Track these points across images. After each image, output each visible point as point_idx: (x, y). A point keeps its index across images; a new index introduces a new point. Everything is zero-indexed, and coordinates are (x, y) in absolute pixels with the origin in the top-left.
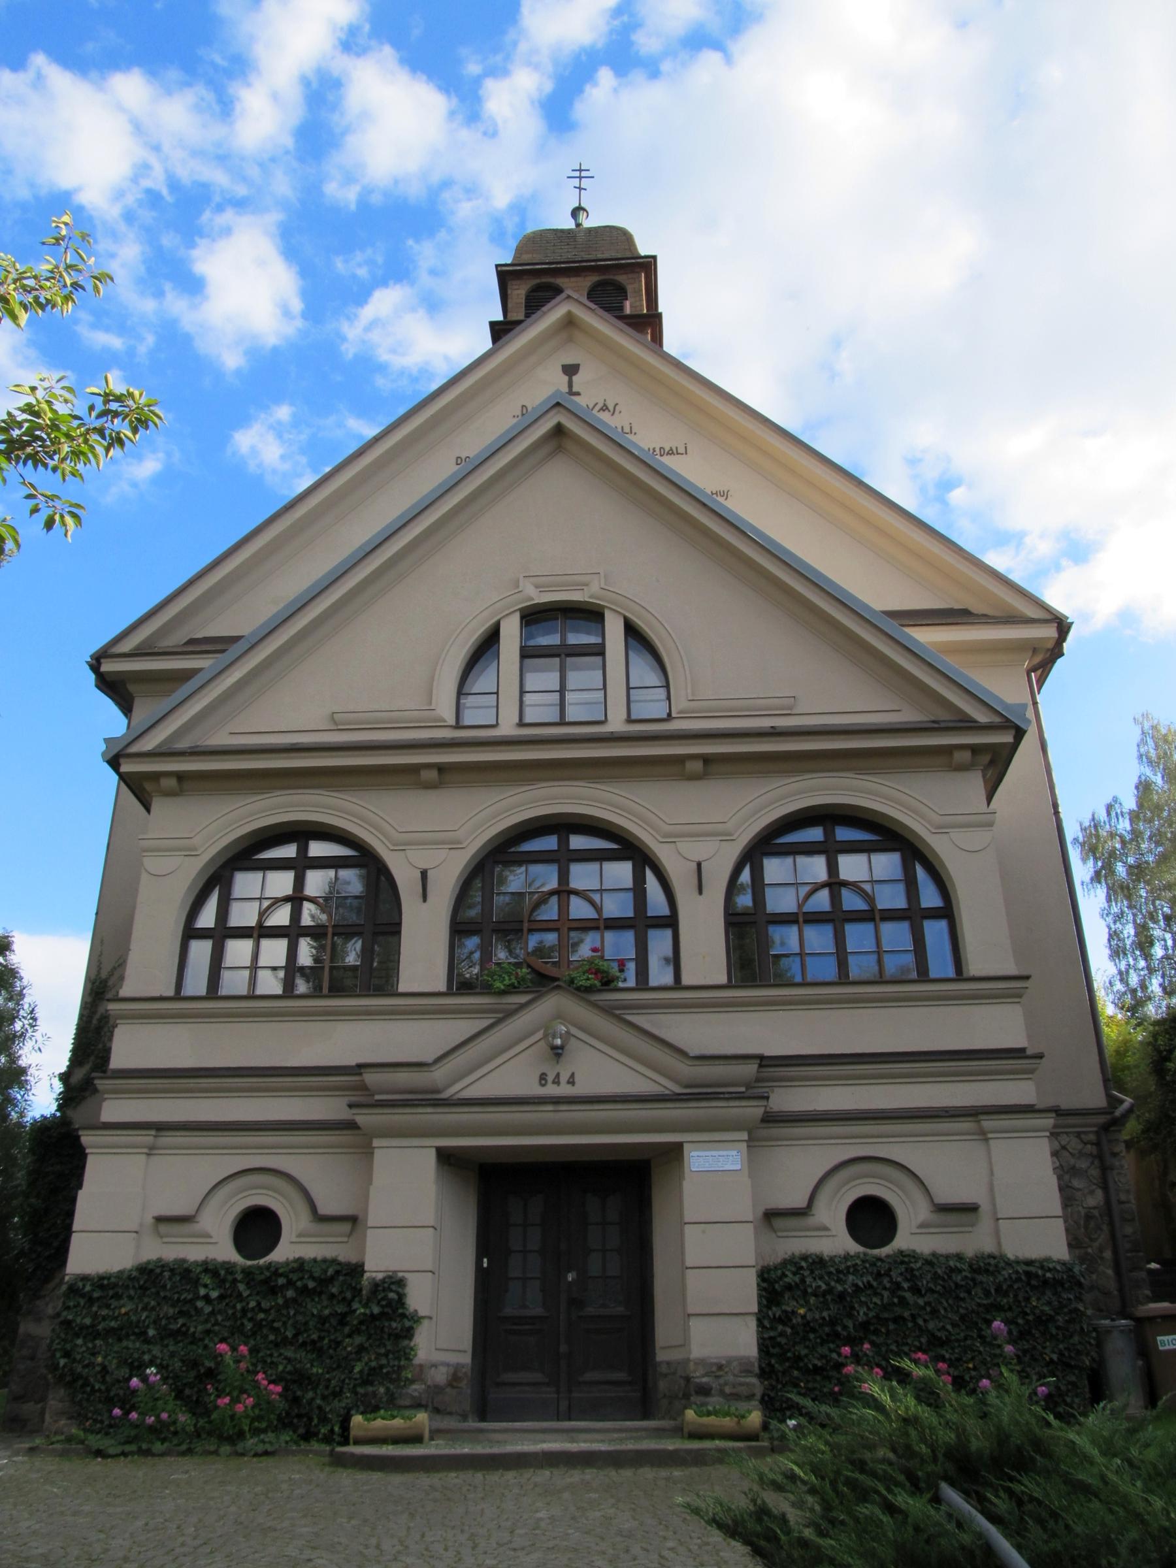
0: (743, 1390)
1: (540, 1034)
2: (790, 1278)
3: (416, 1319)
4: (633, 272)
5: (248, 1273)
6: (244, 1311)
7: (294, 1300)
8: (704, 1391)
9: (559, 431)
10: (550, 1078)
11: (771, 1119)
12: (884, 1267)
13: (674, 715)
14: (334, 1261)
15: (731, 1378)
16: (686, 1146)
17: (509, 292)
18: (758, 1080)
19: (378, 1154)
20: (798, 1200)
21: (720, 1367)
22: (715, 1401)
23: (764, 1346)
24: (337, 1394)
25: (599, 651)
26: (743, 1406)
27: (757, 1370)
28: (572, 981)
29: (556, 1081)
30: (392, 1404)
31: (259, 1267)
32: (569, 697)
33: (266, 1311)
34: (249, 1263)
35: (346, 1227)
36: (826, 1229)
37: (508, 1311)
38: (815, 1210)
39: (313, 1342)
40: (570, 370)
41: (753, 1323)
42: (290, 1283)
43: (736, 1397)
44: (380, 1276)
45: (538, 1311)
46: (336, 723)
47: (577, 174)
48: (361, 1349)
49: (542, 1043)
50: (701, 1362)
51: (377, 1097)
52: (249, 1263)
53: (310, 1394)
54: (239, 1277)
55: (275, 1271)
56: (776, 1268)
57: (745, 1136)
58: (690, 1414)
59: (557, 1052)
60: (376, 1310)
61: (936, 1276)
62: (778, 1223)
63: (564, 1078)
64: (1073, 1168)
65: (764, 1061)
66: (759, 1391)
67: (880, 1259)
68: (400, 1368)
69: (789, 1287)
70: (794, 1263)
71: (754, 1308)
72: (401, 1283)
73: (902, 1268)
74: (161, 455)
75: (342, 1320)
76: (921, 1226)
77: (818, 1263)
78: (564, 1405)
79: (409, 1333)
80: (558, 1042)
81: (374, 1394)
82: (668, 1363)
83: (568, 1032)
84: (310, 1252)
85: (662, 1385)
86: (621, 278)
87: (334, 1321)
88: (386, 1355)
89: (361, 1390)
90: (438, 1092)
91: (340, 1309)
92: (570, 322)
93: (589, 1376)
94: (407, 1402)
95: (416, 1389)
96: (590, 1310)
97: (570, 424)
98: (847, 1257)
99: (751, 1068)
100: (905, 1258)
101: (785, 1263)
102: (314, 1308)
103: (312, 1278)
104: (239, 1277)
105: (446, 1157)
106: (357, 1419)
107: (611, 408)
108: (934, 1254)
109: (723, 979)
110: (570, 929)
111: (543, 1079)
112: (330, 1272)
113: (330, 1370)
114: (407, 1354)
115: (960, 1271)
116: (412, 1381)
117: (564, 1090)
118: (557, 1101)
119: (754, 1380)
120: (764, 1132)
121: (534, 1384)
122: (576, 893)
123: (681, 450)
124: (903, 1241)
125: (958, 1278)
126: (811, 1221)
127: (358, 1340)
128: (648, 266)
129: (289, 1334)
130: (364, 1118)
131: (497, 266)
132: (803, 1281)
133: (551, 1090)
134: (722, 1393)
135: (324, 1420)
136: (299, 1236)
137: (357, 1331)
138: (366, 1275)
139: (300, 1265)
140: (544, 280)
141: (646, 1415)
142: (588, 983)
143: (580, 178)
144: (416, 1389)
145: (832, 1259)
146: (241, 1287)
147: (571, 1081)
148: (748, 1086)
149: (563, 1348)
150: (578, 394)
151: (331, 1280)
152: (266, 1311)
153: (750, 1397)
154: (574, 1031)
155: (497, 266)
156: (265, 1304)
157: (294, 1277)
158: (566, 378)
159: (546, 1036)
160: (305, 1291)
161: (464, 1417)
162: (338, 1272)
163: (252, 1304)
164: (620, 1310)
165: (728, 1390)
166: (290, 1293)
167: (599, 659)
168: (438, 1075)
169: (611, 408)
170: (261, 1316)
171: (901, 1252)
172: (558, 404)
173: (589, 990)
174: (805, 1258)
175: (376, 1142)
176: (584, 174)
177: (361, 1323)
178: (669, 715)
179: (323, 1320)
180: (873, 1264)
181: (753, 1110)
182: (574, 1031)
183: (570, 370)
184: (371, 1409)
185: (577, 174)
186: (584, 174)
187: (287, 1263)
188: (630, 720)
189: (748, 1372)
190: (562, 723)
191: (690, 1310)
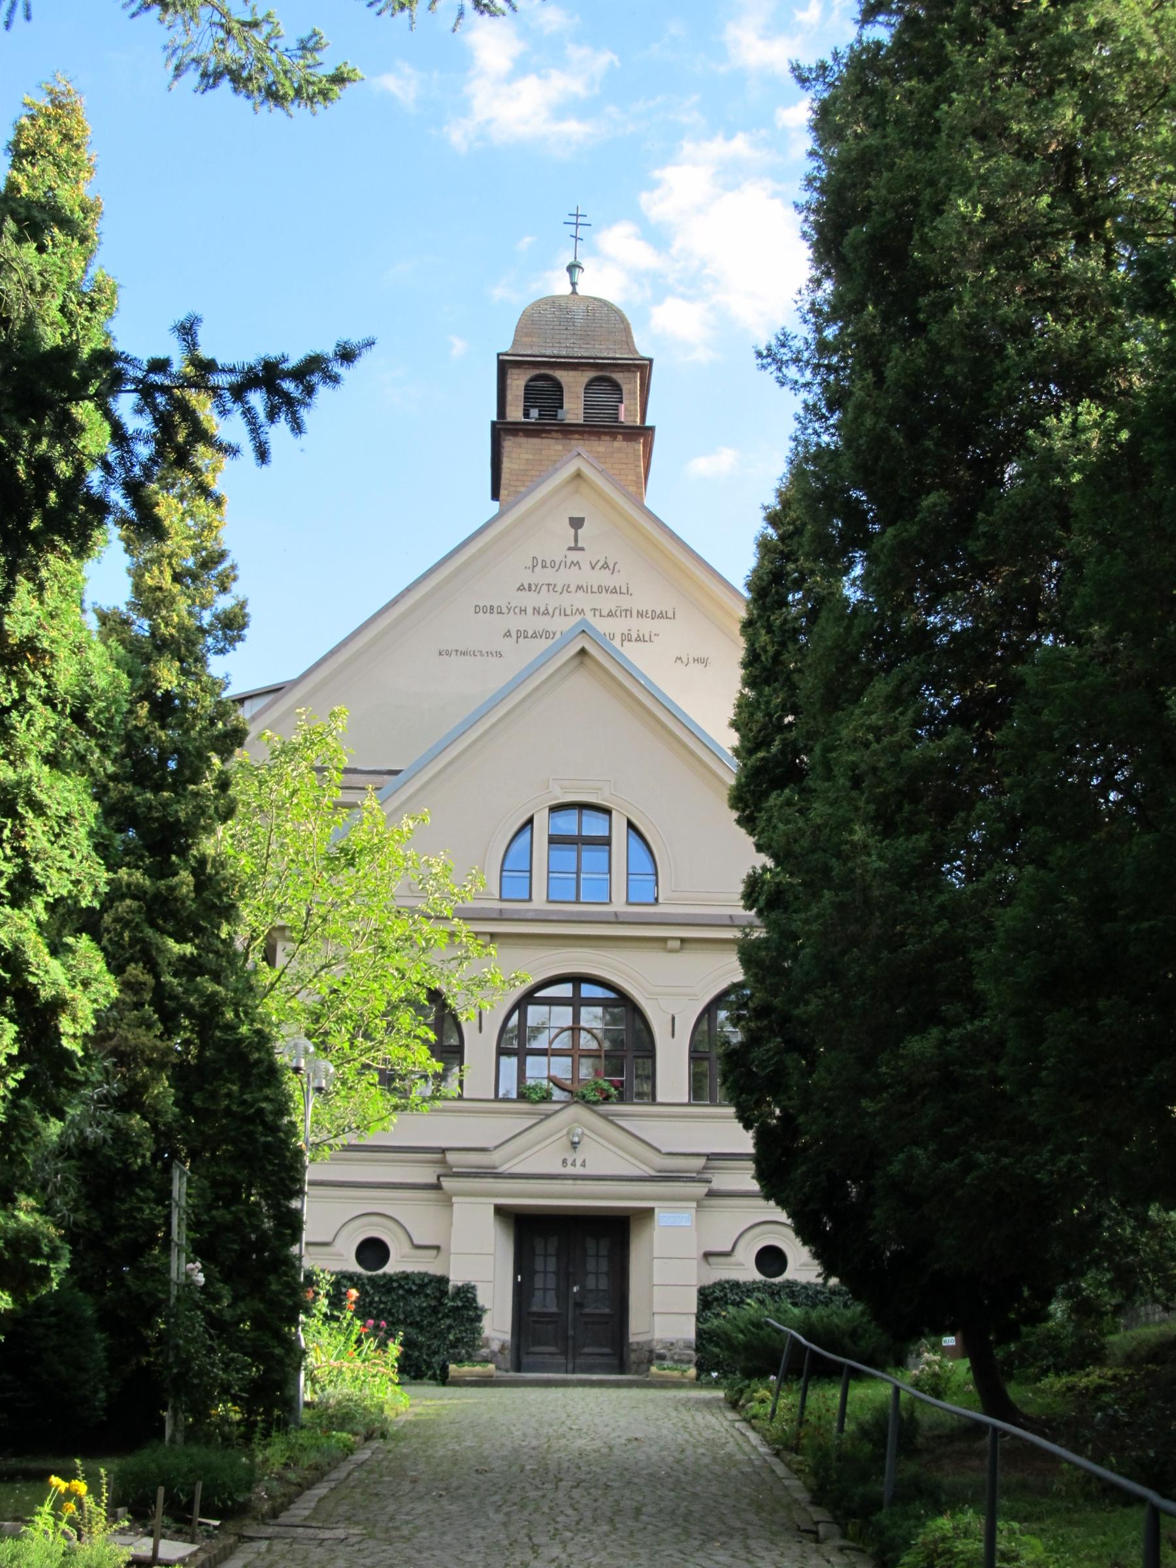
0: (685, 1358)
1: (565, 1132)
2: (718, 1294)
3: (484, 1311)
4: (629, 371)
5: (370, 1278)
6: (371, 1303)
7: (403, 1297)
8: (662, 1357)
9: (583, 652)
10: (569, 1162)
11: (712, 1194)
12: (776, 1289)
13: (660, 900)
14: (426, 1274)
15: (677, 1350)
16: (656, 1211)
17: (509, 382)
18: (705, 1168)
19: (455, 1206)
20: (728, 1248)
21: (672, 1344)
22: (667, 1363)
23: (700, 1333)
24: (436, 1353)
25: (606, 842)
26: (685, 1367)
27: (694, 1346)
28: (584, 1097)
29: (574, 1164)
30: (470, 1358)
31: (377, 1276)
32: (582, 876)
33: (385, 1303)
34: (370, 1273)
35: (433, 1252)
36: (742, 1265)
37: (534, 1309)
38: (736, 1253)
39: (417, 1323)
40: (577, 523)
41: (693, 1319)
42: (401, 1286)
43: (681, 1361)
44: (460, 1284)
45: (554, 1309)
46: (411, 891)
47: (573, 220)
48: (450, 1327)
49: (565, 1139)
50: (660, 1341)
51: (454, 1170)
52: (370, 1273)
53: (417, 1354)
54: (366, 1281)
55: (389, 1279)
56: (709, 1287)
57: (694, 1204)
58: (654, 1369)
59: (574, 1145)
60: (460, 1304)
61: (808, 1296)
62: (712, 1260)
63: (578, 1163)
64: (356, 1342)
65: (710, 1157)
66: (695, 1359)
67: (774, 1284)
68: (475, 1339)
69: (717, 1299)
70: (720, 1285)
71: (695, 1310)
72: (474, 1287)
73: (788, 1290)
74: (68, 406)
75: (435, 1310)
76: (802, 1265)
77: (736, 1285)
78: (570, 1366)
79: (479, 1318)
80: (576, 1139)
81: (459, 1353)
82: (638, 1343)
83: (583, 1133)
84: (411, 1268)
85: (633, 1357)
86: (618, 376)
87: (429, 1311)
88: (466, 1331)
89: (451, 1351)
90: (495, 1168)
91: (433, 1303)
92: (578, 475)
93: (587, 1350)
94: (479, 1359)
95: (484, 1351)
96: (587, 1310)
97: (592, 649)
98: (754, 1282)
99: (702, 1162)
100: (790, 1284)
101: (715, 1284)
102: (416, 1302)
103: (414, 1283)
104: (366, 1281)
105: (500, 1211)
106: (452, 1367)
107: (611, 566)
108: (808, 1283)
109: (686, 1100)
110: (581, 1056)
111: (564, 1162)
112: (426, 1280)
113: (430, 1339)
114: (478, 1331)
115: (823, 1293)
116: (482, 1347)
117: (578, 1170)
118: (575, 1178)
119: (693, 1353)
120: (706, 1203)
121: (550, 1354)
122: (585, 1029)
123: (670, 615)
124: (789, 1274)
125: (821, 1297)
126: (732, 1259)
127: (448, 1321)
128: (643, 368)
129: (402, 1317)
130: (446, 1183)
131: (499, 355)
132: (726, 1295)
133: (569, 1170)
134: (672, 1359)
135: (429, 1366)
136: (403, 1257)
137: (446, 1316)
138: (451, 1284)
139: (406, 1276)
140: (543, 371)
141: (622, 1372)
142: (595, 1099)
143: (577, 224)
144: (484, 1351)
145: (745, 1283)
146: (368, 1288)
147: (583, 1165)
148: (698, 1173)
149: (571, 1333)
150: (582, 549)
151: (426, 1285)
152: (385, 1303)
153: (689, 1362)
154: (587, 1132)
155: (499, 355)
156: (383, 1299)
157: (403, 1283)
158: (572, 531)
159: (568, 1133)
160: (410, 1291)
161: (507, 1371)
162: (431, 1281)
163: (376, 1299)
164: (607, 1311)
165: (676, 1357)
166: (401, 1292)
167: (607, 848)
168: (493, 1158)
169: (611, 566)
170: (382, 1306)
171: (788, 1281)
172: (583, 631)
173: (596, 1103)
174: (727, 1282)
175: (454, 1199)
176: (581, 220)
177: (450, 1311)
178: (657, 899)
179: (422, 1309)
180: (770, 1287)
181: (701, 1189)
182: (587, 1132)
183: (577, 523)
184: (459, 1361)
185: (573, 220)
186: (581, 220)
187: (396, 1274)
188: (628, 903)
189: (689, 1347)
190: (578, 902)
191: (655, 1310)
